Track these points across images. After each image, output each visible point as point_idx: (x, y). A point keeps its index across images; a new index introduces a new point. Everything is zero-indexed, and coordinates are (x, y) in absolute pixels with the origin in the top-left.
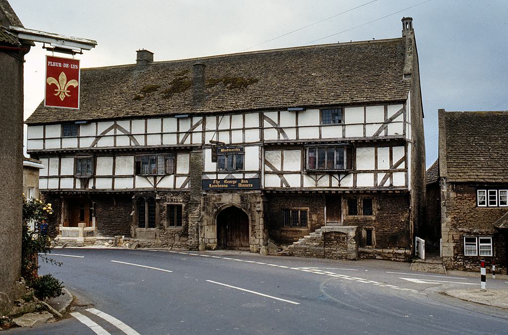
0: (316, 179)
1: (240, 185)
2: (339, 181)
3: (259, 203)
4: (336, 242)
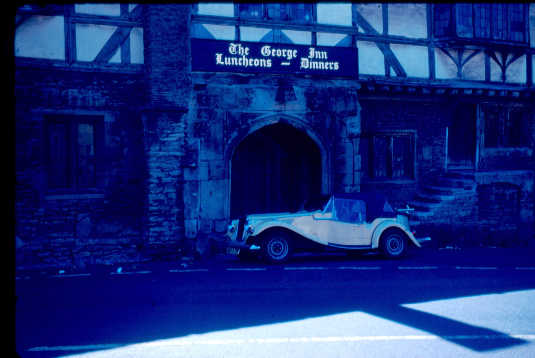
0: (460, 60)
1: (305, 64)
2: (504, 68)
3: (353, 114)
4: (497, 206)
